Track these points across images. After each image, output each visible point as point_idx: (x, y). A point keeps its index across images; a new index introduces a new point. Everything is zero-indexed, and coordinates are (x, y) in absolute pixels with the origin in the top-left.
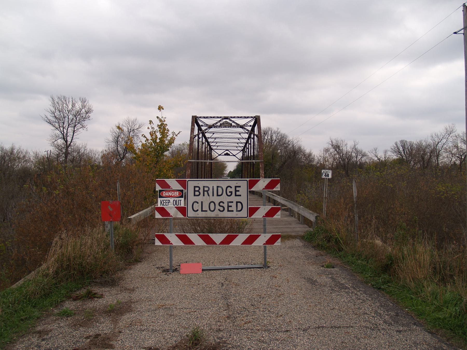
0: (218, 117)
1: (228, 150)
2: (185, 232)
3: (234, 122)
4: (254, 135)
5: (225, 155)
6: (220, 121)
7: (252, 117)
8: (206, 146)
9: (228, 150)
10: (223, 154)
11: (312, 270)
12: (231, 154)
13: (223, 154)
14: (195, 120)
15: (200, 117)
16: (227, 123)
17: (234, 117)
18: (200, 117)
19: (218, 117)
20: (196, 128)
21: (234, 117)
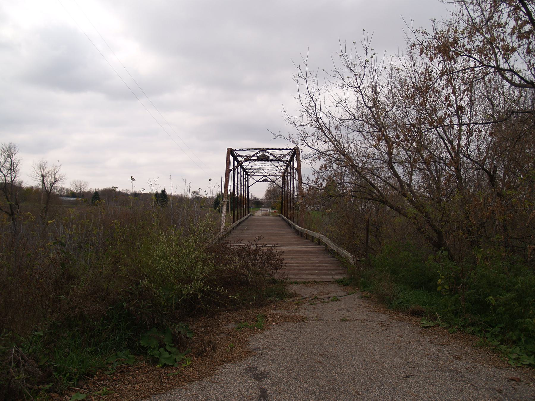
0: (254, 150)
1: (266, 176)
2: (296, 220)
3: (271, 154)
4: (293, 169)
5: (263, 181)
6: (257, 153)
7: (291, 149)
8: (239, 172)
9: (266, 176)
10: (261, 180)
11: (384, 317)
12: (269, 180)
13: (261, 180)
14: (231, 152)
15: (236, 150)
16: (263, 155)
17: (272, 149)
18: (236, 150)
19: (254, 150)
20: (232, 158)
21: (272, 149)
